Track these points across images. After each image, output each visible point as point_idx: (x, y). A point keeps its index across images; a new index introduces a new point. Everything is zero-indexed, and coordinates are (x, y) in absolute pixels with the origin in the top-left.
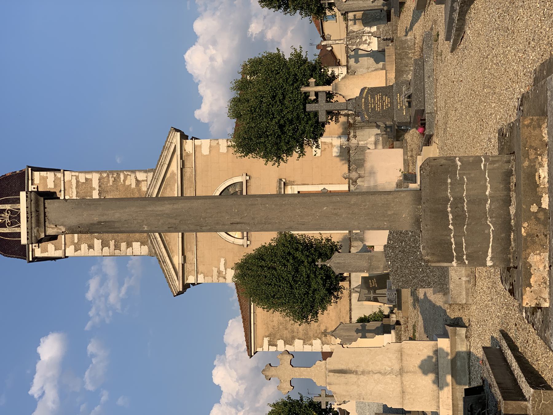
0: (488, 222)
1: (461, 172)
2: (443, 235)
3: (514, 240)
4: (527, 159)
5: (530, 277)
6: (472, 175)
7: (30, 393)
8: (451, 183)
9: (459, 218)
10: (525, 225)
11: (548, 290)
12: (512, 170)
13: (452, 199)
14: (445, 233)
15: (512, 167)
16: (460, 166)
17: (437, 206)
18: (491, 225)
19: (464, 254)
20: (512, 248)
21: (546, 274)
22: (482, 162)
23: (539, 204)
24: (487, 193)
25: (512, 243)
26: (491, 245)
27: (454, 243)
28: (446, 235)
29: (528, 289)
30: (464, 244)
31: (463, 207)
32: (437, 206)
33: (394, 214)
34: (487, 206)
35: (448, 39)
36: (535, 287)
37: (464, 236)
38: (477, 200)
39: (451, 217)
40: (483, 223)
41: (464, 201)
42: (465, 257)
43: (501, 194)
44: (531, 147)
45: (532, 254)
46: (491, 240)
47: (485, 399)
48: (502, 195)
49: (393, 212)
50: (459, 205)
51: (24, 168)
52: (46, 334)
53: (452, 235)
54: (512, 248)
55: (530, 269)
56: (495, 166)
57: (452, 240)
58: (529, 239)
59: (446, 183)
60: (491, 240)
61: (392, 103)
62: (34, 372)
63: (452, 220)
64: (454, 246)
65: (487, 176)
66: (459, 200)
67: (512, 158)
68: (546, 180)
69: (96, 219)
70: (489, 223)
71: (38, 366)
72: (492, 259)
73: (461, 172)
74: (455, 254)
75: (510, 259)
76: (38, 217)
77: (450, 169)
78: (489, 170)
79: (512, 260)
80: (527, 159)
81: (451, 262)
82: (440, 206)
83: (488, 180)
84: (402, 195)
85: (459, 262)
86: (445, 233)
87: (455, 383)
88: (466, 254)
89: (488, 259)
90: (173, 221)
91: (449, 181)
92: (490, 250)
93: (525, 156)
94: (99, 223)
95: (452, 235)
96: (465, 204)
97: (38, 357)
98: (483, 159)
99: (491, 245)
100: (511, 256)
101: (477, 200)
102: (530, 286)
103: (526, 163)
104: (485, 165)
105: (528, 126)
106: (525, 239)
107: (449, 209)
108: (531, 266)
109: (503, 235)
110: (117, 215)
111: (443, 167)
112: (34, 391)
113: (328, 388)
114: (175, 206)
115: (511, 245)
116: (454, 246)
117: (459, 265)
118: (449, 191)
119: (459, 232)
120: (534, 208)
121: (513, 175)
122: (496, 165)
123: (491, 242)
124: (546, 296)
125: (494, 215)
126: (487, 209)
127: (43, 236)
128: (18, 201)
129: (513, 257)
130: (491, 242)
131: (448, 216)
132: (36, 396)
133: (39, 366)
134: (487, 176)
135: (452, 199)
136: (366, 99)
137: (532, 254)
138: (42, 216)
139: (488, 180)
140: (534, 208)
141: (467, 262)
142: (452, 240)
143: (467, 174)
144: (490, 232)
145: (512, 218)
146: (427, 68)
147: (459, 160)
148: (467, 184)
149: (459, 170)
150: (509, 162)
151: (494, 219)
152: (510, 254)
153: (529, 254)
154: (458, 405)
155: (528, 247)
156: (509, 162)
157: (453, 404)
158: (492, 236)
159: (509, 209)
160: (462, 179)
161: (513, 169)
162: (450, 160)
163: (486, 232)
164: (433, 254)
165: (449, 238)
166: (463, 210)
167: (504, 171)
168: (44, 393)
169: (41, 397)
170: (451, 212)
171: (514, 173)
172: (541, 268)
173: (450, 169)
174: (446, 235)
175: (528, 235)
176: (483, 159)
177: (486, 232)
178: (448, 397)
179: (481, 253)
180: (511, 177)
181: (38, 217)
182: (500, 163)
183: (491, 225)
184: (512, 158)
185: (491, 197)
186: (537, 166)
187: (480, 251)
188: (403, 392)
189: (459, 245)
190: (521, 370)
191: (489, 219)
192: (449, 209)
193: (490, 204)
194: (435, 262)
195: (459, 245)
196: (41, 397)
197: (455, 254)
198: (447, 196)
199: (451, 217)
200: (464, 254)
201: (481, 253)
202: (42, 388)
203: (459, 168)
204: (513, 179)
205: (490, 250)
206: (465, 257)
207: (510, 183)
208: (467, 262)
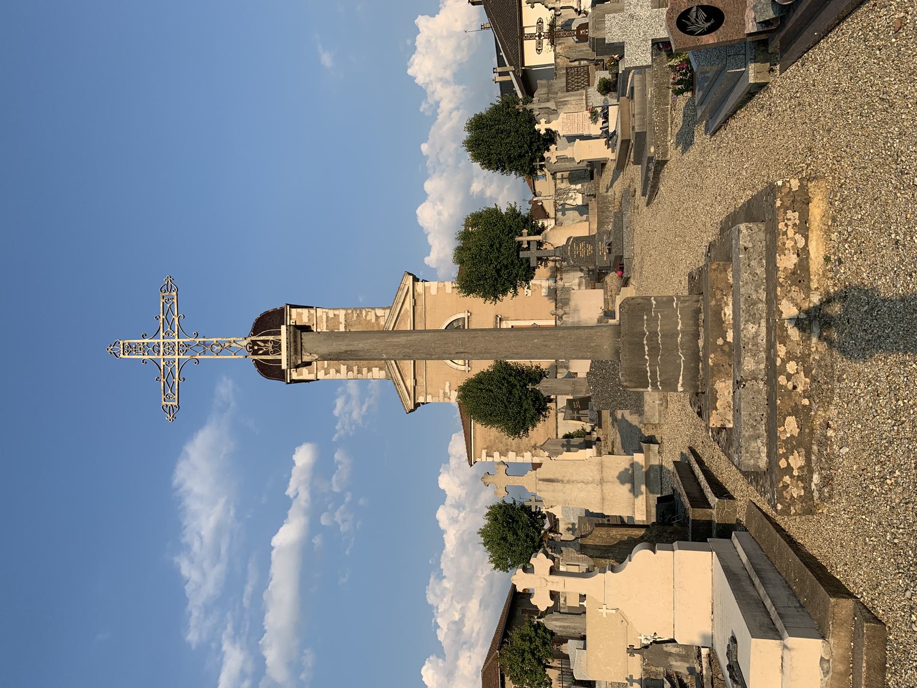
9: (654, 350)
10: (712, 356)
11: (732, 412)
14: (642, 362)
21: (730, 399)
23: (725, 338)
29: (714, 411)
34: (679, 339)
35: (644, 194)
36: (720, 410)
39: (646, 348)
44: (718, 288)
51: (283, 305)
52: (300, 444)
61: (594, 250)
62: (290, 476)
64: (649, 374)
68: (731, 317)
69: (343, 348)
72: (682, 385)
76: (296, 346)
86: (642, 362)
89: (679, 385)
90: (405, 350)
91: (645, 317)
92: (681, 378)
94: (346, 352)
97: (293, 464)
102: (716, 409)
103: (713, 303)
104: (677, 304)
105: (715, 270)
106: (712, 369)
110: (361, 345)
112: (290, 492)
114: (409, 338)
116: (649, 374)
120: (720, 342)
124: (731, 418)
127: (299, 362)
128: (279, 333)
132: (291, 496)
136: (572, 246)
138: (299, 346)
140: (720, 342)
146: (625, 220)
156: (698, 301)
160: (656, 316)
164: (631, 381)
166: (658, 343)
168: (298, 494)
172: (726, 394)
175: (715, 364)
181: (296, 346)
185: (682, 331)
186: (723, 305)
189: (654, 373)
192: (645, 342)
195: (654, 373)
199: (646, 348)
205: (681, 378)
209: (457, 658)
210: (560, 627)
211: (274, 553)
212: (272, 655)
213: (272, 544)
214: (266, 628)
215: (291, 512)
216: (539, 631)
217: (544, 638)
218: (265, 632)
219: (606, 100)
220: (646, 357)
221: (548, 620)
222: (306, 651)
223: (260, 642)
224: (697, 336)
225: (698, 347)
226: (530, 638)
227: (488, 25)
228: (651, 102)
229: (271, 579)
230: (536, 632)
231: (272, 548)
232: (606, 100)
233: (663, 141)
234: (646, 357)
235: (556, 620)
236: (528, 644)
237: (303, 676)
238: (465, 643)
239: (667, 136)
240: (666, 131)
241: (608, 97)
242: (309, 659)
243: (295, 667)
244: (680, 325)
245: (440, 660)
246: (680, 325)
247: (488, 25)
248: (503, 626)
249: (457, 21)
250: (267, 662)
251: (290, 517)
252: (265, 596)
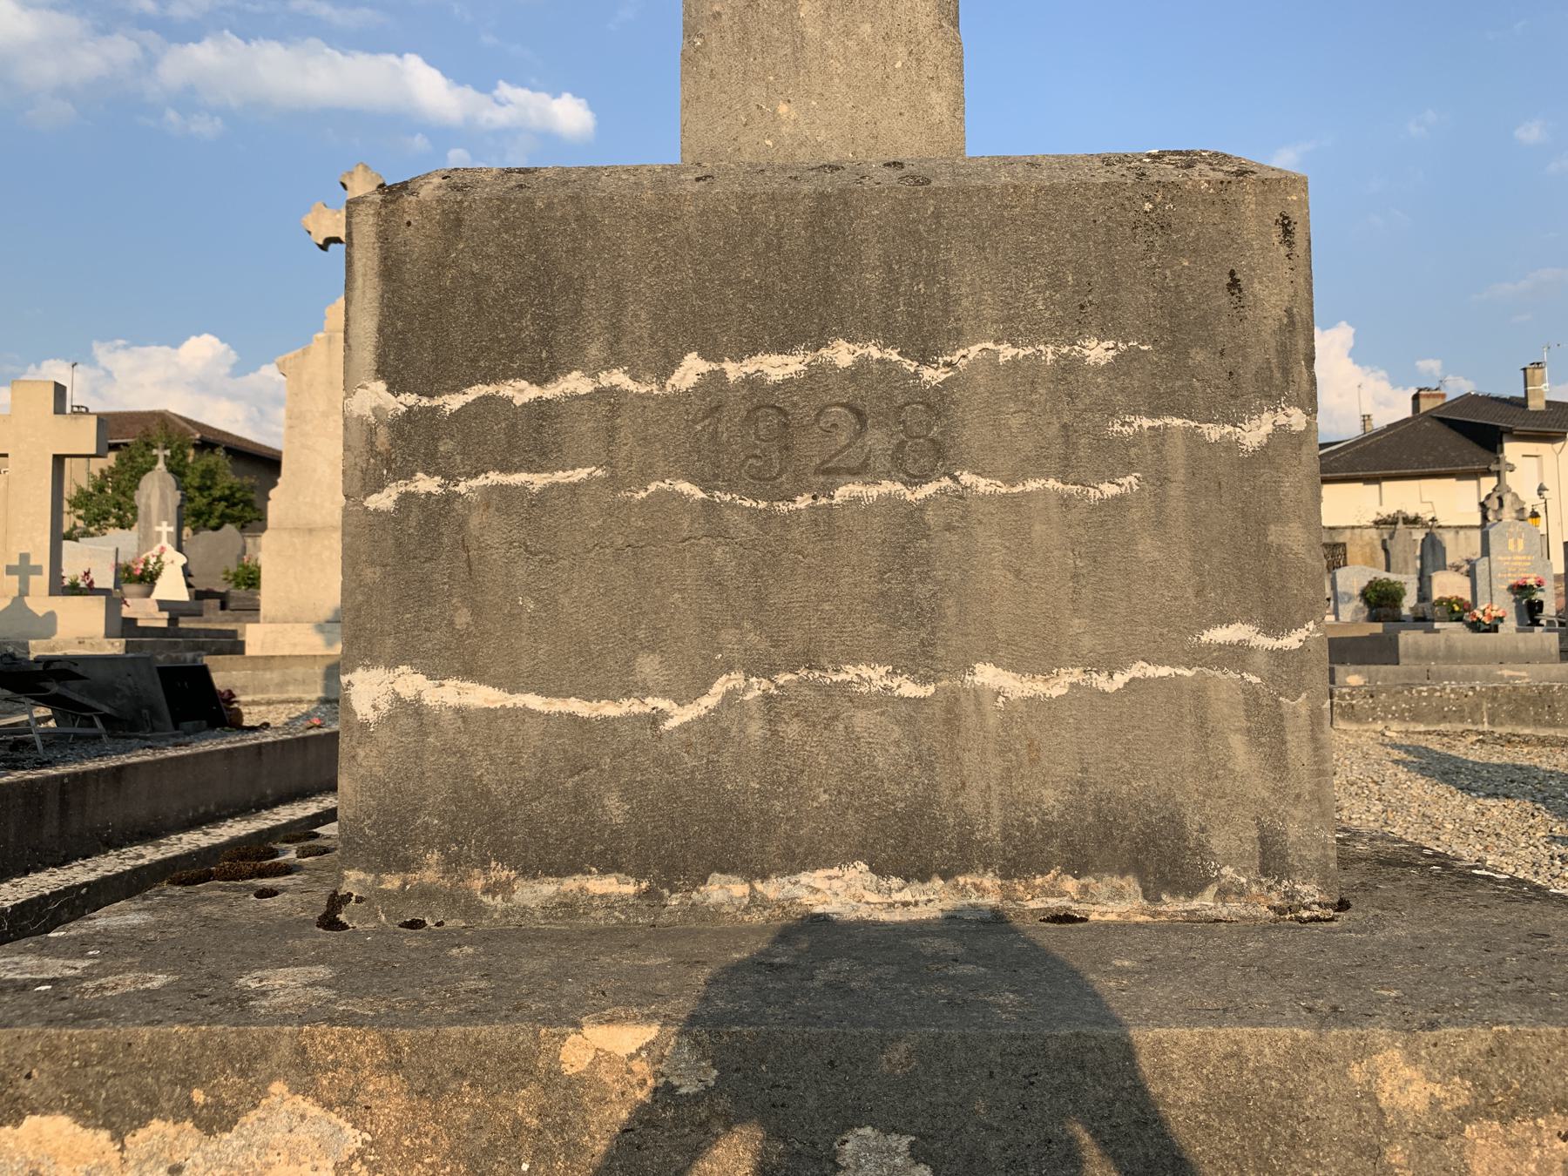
0: (736, 679)
1: (1177, 453)
2: (620, 306)
3: (568, 906)
4: (1461, 1093)
5: (88, 1112)
6: (1147, 548)
7: (501, 83)
8: (1070, 368)
9: (764, 441)
12: (1194, 890)
13: (933, 375)
14: (639, 321)
15: (1223, 894)
16: (1231, 446)
17: (873, 254)
18: (710, 701)
19: (450, 477)
20: (503, 888)
22: (1273, 627)
24: (987, 675)
25: (548, 888)
26: (535, 702)
27: (551, 391)
28: (616, 331)
30: (539, 481)
31: (860, 471)
32: (873, 254)
33: (799, 42)
34: (875, 676)
37: (614, 482)
38: (922, 590)
39: (778, 367)
40: (728, 636)
41: (914, 480)
42: (426, 484)
43: (980, 793)
45: (353, 1138)
46: (577, 706)
47: (153, 730)
48: (972, 800)
49: (813, 32)
50: (877, 440)
52: (592, 107)
53: (618, 378)
54: (503, 888)
55: (183, 1110)
56: (1238, 742)
57: (575, 383)
58: (524, 1104)
59: (1077, 322)
60: (577, 706)
62: (533, 89)
63: (753, 383)
64: (521, 392)
65: (1139, 670)
66: (924, 434)
67: (1309, 891)
70: (720, 687)
71: (544, 96)
72: (411, 710)
73: (1177, 453)
74: (454, 402)
75: (405, 866)
77: (1198, 356)
78: (1199, 692)
79: (392, 882)
80: (1461, 1093)
81: (381, 372)
82: (872, 279)
83: (1101, 682)
84: (935, 97)
85: (383, 439)
86: (639, 321)
87: (329, 662)
88: (449, 499)
89: (410, 682)
91: (1097, 352)
92: (482, 696)
93: (1496, 1072)
95: (618, 378)
96: (887, 487)
97: (556, 95)
98: (1292, 641)
99: (535, 702)
100: (430, 876)
101: (922, 590)
104: (1237, 655)
106: (518, 1067)
107: (842, 354)
108: (215, 1121)
109: (615, 808)
111: (1224, 299)
112: (505, 90)
113: (320, 335)
115: (530, 871)
117: (359, 444)
118: (1007, 352)
119: (645, 441)
121: (1151, 896)
122: (1240, 753)
123: (558, 706)
125: (792, 730)
126: (849, 673)
129: (426, 893)
130: (558, 706)
131: (783, 347)
132: (496, 93)
133: (542, 98)
134: (1139, 670)
135: (933, 375)
137: (353, 1138)
139: (1101, 682)
141: (383, 501)
142: (575, 383)
143: (1160, 500)
144: (646, 691)
145: (772, 889)
147: (1280, 432)
148: (1065, 502)
149: (1192, 437)
150: (1272, 859)
151: (756, 729)
152: (452, 863)
153: (347, 1103)
154: (271, 669)
155: (429, 1089)
156: (1272, 859)
157: (273, 657)
158: (610, 710)
159: (848, 859)
161: (1206, 902)
162: (1284, 351)
163: (648, 666)
165: (594, 351)
166: (832, 473)
167: (1193, 821)
168: (502, 105)
169: (496, 101)
170: (816, 374)
171: (1174, 906)
173: (1198, 356)
174: (616, 331)
176: (1292, 641)
177: (648, 666)
178: (295, 645)
179: (463, 618)
180: (1131, 884)
182: (1260, 788)
183: (710, 701)
184: (1309, 891)
185: (951, 713)
187: (477, 611)
188: (311, 531)
189: (535, 438)
190: (175, 858)
191: (758, 687)
192: (842, 354)
193: (885, 699)
194: (384, 238)
195: (535, 438)
196: (496, 101)
197: (454, 402)
198: (958, 338)
199: (778, 367)
200: (450, 477)
201: (463, 618)
202: (510, 102)
203: (1213, 432)
204: (1119, 894)
205: (482, 696)
206: (426, 484)
207: (1078, 868)
208: (383, 501)
209: (233, 397)
210: (148, 506)
211: (392, 59)
212: (205, 56)
213: (407, 56)
214: (254, 44)
215: (469, 93)
216: (224, 504)
217: (210, 514)
218: (247, 42)
219: (1351, 598)
220: (691, 370)
221: (162, 480)
222: (218, 121)
223: (226, 32)
224: (906, 850)
225: (796, 860)
226: (209, 488)
227: (1368, 428)
228: (1488, 677)
229: (344, 54)
230: (220, 499)
231: (400, 55)
232: (1351, 598)
233: (1386, 710)
234: (691, 370)
235: (163, 497)
236: (196, 482)
237: (172, 115)
238: (260, 411)
239: (1402, 719)
240: (1416, 718)
241: (1358, 603)
242: (206, 128)
243: (188, 100)
244: (1017, 686)
245: (228, 370)
246: (1017, 686)
247: (1368, 428)
248: (250, 449)
249: (1340, 396)
250: (191, 45)
251: (460, 89)
252: (313, 42)
